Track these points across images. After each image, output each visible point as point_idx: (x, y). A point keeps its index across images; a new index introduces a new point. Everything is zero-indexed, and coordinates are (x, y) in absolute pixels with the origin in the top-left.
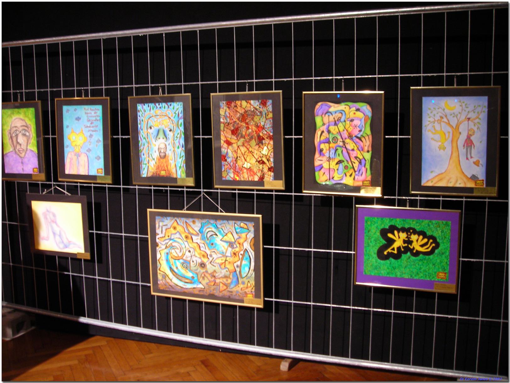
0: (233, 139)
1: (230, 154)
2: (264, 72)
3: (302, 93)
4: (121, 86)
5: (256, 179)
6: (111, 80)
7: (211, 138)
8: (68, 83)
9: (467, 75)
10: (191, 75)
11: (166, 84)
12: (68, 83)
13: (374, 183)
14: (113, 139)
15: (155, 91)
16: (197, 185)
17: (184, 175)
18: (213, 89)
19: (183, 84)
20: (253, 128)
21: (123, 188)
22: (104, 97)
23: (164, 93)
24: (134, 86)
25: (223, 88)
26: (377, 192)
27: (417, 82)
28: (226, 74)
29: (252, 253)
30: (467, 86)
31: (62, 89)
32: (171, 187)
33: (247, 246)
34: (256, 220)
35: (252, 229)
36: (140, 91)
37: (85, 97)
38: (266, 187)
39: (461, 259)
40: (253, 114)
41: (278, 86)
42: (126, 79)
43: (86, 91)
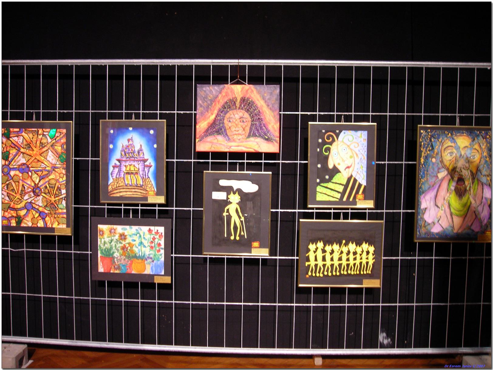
3: (308, 124)
4: (105, 111)
6: (82, 104)
7: (99, 160)
8: (115, 104)
9: (73, 110)
10: (380, 106)
11: (107, 111)
12: (431, 107)
13: (158, 194)
16: (168, 202)
18: (103, 116)
19: (124, 111)
21: (141, 209)
24: (90, 111)
26: (369, 204)
27: (313, 118)
28: (327, 106)
30: (421, 124)
31: (41, 111)
32: (109, 204)
37: (36, 120)
38: (358, 206)
41: (162, 116)
42: (99, 104)
43: (38, 114)
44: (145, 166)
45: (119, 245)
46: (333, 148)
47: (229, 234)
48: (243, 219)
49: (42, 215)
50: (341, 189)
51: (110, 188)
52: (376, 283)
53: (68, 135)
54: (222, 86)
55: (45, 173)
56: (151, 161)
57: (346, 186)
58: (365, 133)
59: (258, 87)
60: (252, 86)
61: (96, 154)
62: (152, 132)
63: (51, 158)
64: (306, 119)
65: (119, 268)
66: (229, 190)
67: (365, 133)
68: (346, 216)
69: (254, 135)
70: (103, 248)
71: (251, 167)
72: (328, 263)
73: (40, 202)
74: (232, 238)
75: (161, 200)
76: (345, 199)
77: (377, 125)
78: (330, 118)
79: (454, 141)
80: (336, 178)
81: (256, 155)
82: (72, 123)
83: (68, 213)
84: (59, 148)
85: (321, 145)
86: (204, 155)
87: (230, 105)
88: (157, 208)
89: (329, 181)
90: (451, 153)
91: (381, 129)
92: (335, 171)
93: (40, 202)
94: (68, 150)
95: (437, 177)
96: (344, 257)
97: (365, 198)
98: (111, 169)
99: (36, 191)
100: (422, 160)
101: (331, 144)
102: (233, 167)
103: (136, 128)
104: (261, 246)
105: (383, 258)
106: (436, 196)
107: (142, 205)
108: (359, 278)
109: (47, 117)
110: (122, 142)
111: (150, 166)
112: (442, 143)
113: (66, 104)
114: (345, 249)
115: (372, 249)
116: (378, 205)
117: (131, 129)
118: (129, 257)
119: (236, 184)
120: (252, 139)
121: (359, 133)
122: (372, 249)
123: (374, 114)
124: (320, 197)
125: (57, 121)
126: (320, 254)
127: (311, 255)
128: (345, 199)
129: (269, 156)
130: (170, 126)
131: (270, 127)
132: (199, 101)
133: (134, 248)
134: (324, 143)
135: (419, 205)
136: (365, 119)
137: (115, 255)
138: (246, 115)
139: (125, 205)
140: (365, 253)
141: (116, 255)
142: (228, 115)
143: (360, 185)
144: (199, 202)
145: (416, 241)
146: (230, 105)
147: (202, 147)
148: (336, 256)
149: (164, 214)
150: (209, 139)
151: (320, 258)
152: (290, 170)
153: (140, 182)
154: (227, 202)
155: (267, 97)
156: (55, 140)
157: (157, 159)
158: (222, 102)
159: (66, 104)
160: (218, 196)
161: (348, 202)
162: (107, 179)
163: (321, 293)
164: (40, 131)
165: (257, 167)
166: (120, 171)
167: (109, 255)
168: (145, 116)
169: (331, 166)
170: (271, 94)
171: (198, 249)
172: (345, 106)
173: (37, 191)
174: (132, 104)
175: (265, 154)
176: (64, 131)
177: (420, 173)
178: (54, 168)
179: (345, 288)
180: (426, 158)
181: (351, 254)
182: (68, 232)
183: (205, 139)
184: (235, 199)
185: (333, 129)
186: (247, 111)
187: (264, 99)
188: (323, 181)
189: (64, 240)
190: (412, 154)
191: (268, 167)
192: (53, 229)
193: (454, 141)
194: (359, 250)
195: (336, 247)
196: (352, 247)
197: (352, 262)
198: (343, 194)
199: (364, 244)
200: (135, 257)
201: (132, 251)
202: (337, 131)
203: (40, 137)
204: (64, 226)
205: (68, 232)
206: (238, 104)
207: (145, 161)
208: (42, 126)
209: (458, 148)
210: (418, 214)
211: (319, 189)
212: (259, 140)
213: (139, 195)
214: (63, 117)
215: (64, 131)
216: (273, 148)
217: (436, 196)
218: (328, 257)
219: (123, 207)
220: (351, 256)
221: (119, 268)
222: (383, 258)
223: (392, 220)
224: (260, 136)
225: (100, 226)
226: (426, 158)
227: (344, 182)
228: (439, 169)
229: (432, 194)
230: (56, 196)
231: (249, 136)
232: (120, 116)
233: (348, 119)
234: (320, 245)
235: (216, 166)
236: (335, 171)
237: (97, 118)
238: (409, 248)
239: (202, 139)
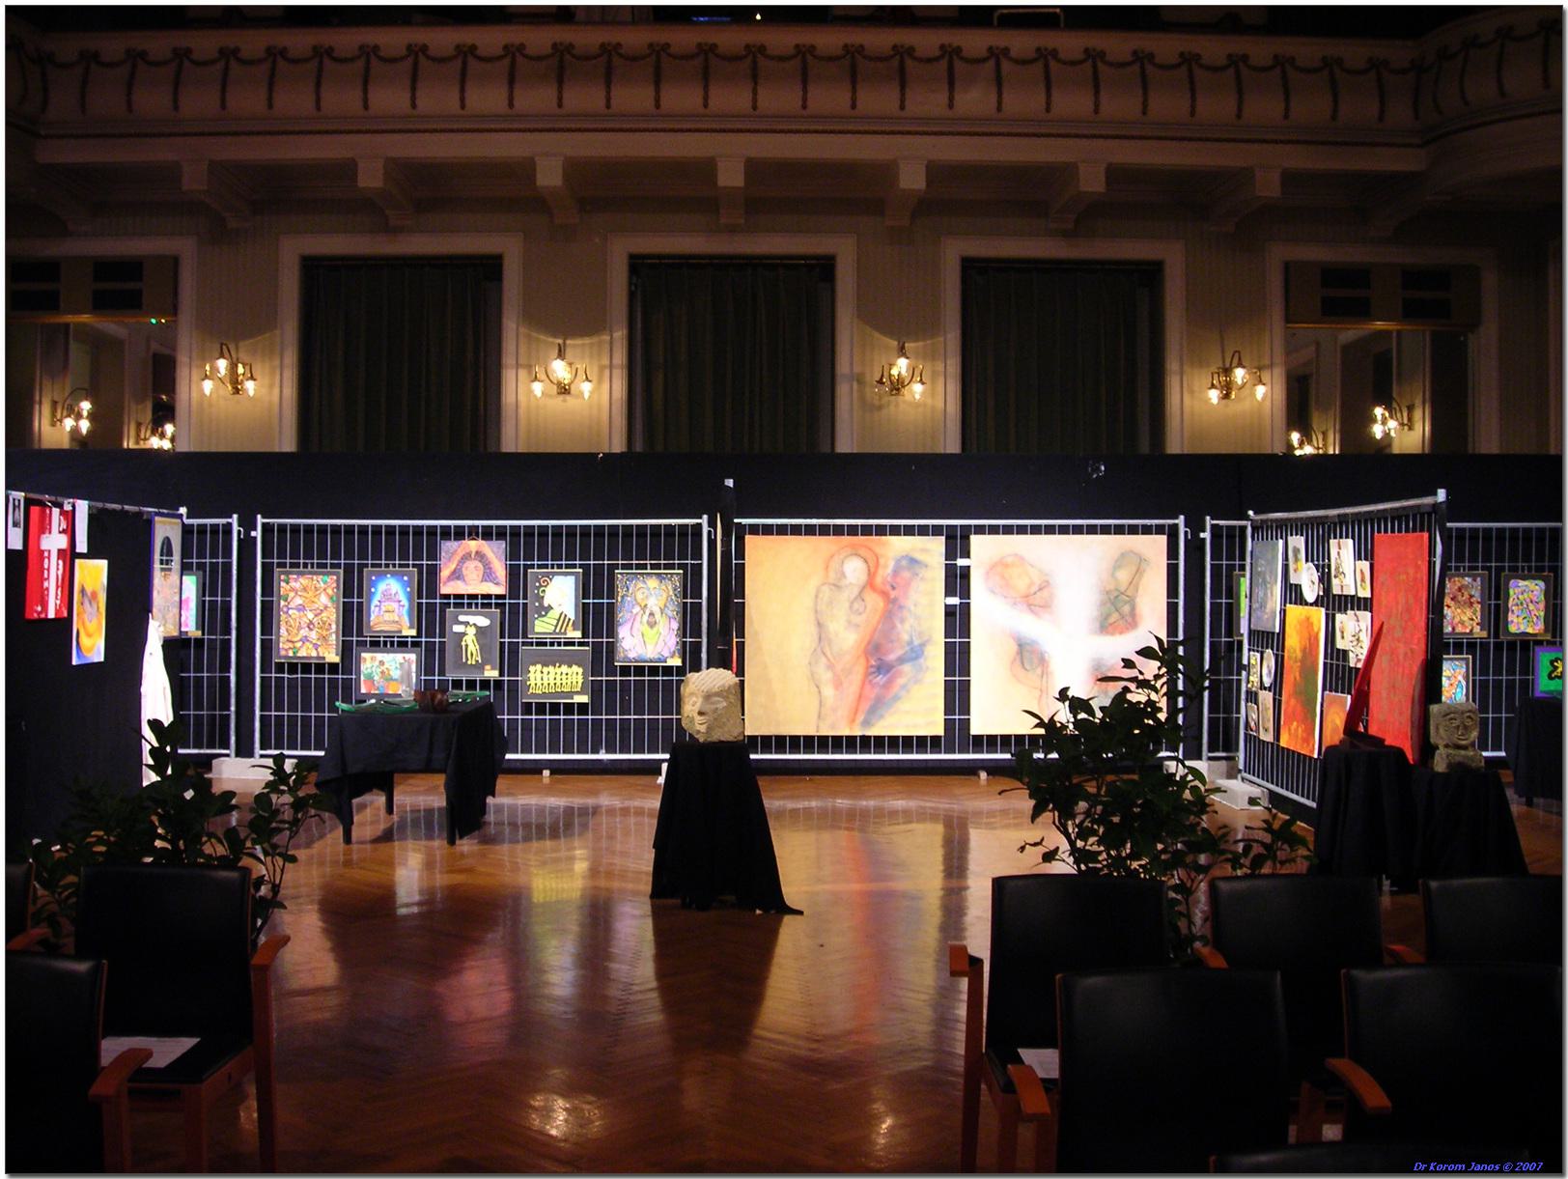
0: (1452, 604)
1: (1449, 614)
2: (571, 556)
5: (1468, 631)
8: (377, 556)
10: (418, 556)
13: (411, 627)
14: (450, 595)
15: (305, 565)
16: (419, 635)
17: (194, 629)
18: (367, 565)
20: (1466, 596)
22: (411, 569)
23: (1464, 570)
25: (624, 567)
26: (578, 634)
27: (532, 567)
28: (543, 556)
29: (1464, 683)
32: (371, 637)
33: (1460, 678)
34: (1467, 660)
35: (1464, 666)
36: (282, 565)
39: (423, 678)
40: (1466, 587)
41: (414, 566)
42: (363, 556)
43: (312, 564)
44: (400, 606)
45: (379, 670)
46: (547, 589)
47: (467, 659)
48: (478, 647)
49: (316, 646)
50: (555, 622)
51: (372, 624)
52: (584, 699)
53: (338, 581)
54: (460, 542)
55: (319, 611)
56: (405, 602)
57: (559, 620)
58: (573, 577)
59: (489, 542)
60: (484, 542)
61: (360, 596)
62: (374, 578)
63: (324, 599)
64: (526, 567)
65: (378, 689)
66: (466, 624)
67: (573, 577)
68: (559, 644)
69: (486, 581)
70: (366, 672)
71: (484, 605)
72: (546, 683)
73: (313, 635)
74: (469, 662)
75: (413, 632)
76: (557, 631)
77: (583, 573)
78: (546, 566)
79: (644, 582)
80: (550, 614)
81: (488, 596)
82: (341, 571)
83: (337, 645)
84: (330, 591)
85: (538, 588)
86: (447, 597)
87: (467, 557)
88: (368, 639)
89: (544, 616)
90: (643, 593)
91: (586, 574)
92: (550, 608)
93: (313, 635)
94: (337, 595)
95: (632, 612)
96: (558, 677)
97: (574, 630)
98: (372, 608)
99: (310, 625)
100: (619, 599)
101: (546, 586)
102: (470, 605)
103: (393, 574)
104: (493, 668)
105: (591, 678)
106: (631, 628)
107: (398, 637)
108: (571, 694)
109: (319, 566)
110: (382, 586)
111: (403, 606)
112: (635, 586)
113: (336, 555)
114: (558, 670)
115: (580, 670)
116: (585, 635)
117: (389, 576)
118: (386, 680)
119: (472, 619)
120: (484, 583)
121: (569, 577)
122: (580, 670)
123: (429, 563)
124: (537, 629)
125: (288, 569)
126: (539, 675)
127: (531, 675)
128: (557, 631)
129: (498, 597)
130: (420, 573)
131: (498, 574)
132: (443, 554)
133: (391, 673)
134: (541, 586)
135: (617, 635)
136: (574, 566)
137: (375, 678)
138: (480, 565)
139: (384, 637)
140: (575, 674)
141: (376, 678)
142: (465, 565)
143: (569, 619)
144: (442, 635)
145: (616, 664)
146: (467, 557)
147: (445, 590)
148: (552, 676)
149: (416, 644)
150: (452, 583)
151: (539, 679)
152: (514, 607)
153: (397, 619)
154: (464, 634)
155: (495, 550)
156: (1300, 600)
157: (410, 600)
158: (461, 554)
159: (336, 555)
160: (457, 629)
161: (560, 633)
162: (369, 616)
163: (541, 708)
164: (315, 577)
165: (489, 605)
166: (380, 610)
167: (370, 678)
168: (400, 566)
169: (546, 605)
170: (499, 548)
171: (442, 672)
172: (557, 556)
173: (311, 626)
174: (390, 556)
175: (468, 595)
176: (335, 577)
177: (617, 609)
178: (326, 607)
179: (560, 703)
180: (622, 597)
181: (564, 675)
182: (336, 659)
183: (449, 584)
184: (471, 631)
185: (547, 575)
186: (480, 561)
187: (493, 552)
188: (541, 616)
189: (333, 667)
190: (612, 594)
191: (497, 605)
192: (324, 658)
193: (644, 582)
194: (570, 671)
195: (551, 668)
196: (564, 668)
197: (564, 682)
198: (556, 626)
199: (574, 666)
200: (392, 679)
201: (389, 675)
202: (550, 576)
203: (315, 582)
204: (334, 655)
205: (336, 659)
206: (473, 556)
207: (400, 601)
208: (316, 573)
209: (649, 589)
210: (617, 641)
211: (536, 622)
212: (490, 584)
213: (396, 629)
214: (333, 566)
215: (335, 577)
216: (501, 590)
217: (631, 628)
218: (545, 678)
219: (382, 639)
220: (564, 677)
221: (378, 689)
222: (591, 678)
223: (597, 648)
224: (491, 581)
225: (363, 655)
226: (622, 597)
227: (557, 617)
228: (633, 605)
229: (629, 625)
230: (327, 630)
231: (482, 581)
232: (380, 566)
233: (560, 566)
234: (539, 667)
235: (456, 605)
236: (550, 608)
237: (361, 567)
238: (611, 671)
239: (445, 583)
